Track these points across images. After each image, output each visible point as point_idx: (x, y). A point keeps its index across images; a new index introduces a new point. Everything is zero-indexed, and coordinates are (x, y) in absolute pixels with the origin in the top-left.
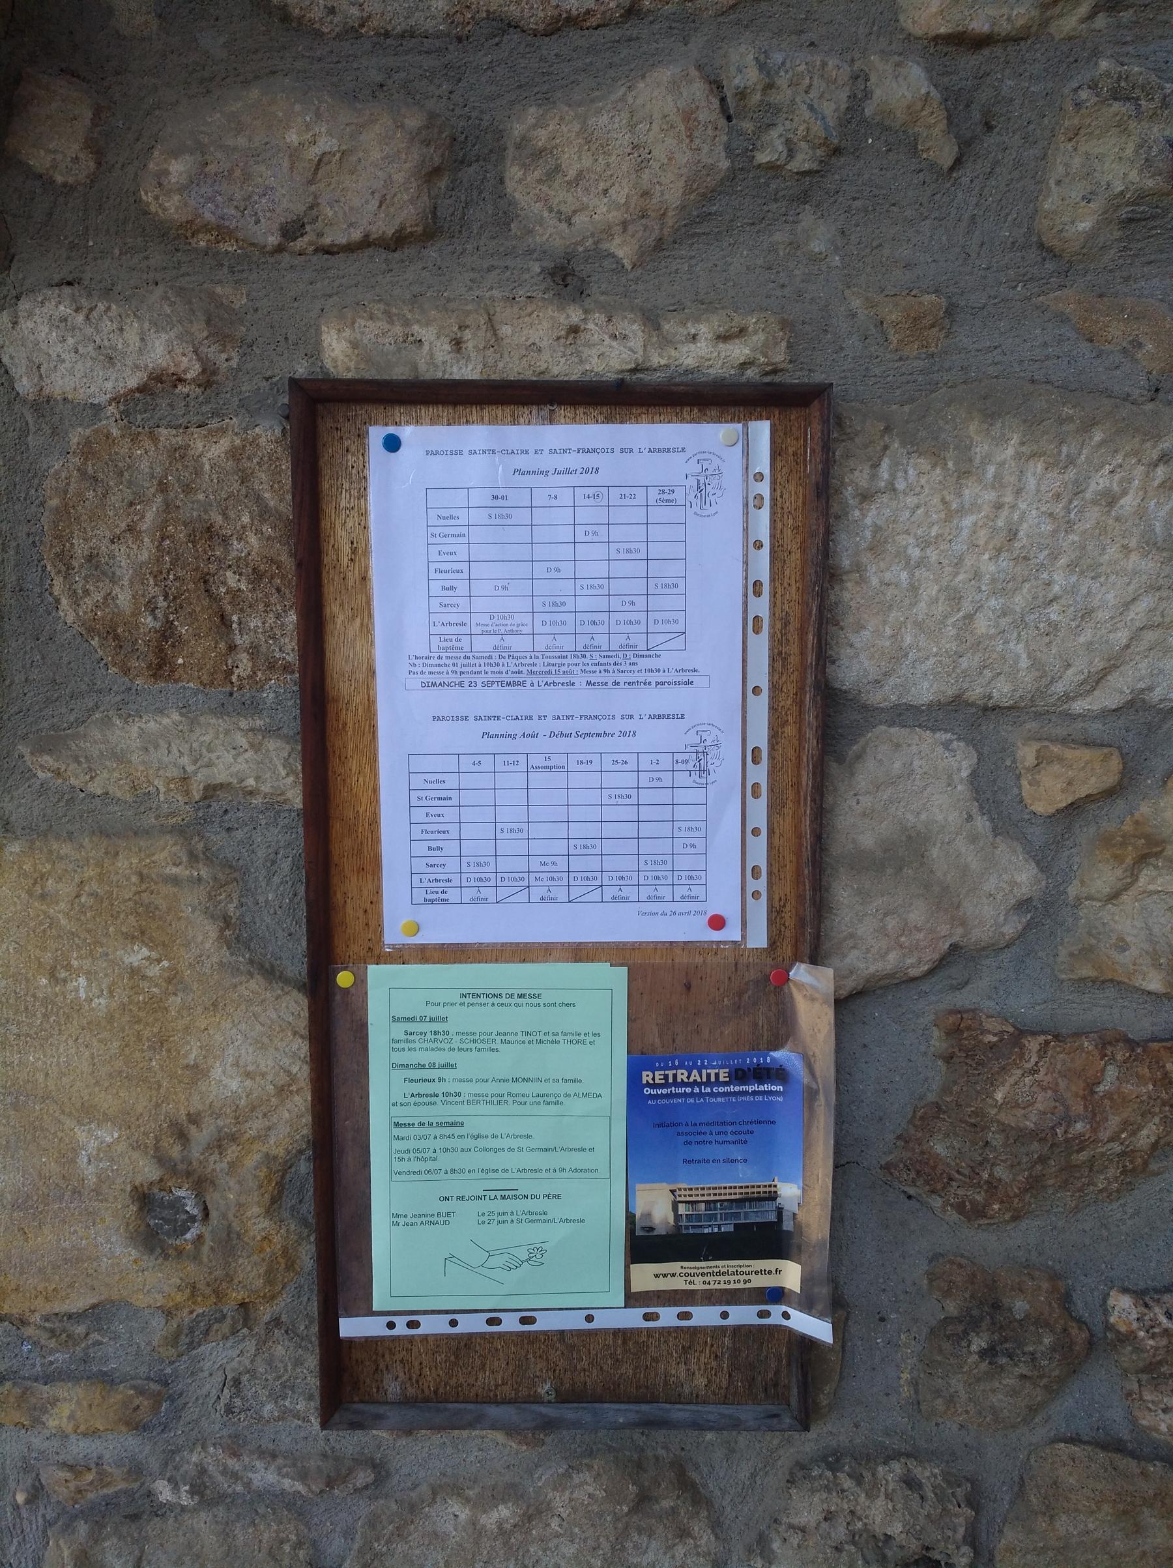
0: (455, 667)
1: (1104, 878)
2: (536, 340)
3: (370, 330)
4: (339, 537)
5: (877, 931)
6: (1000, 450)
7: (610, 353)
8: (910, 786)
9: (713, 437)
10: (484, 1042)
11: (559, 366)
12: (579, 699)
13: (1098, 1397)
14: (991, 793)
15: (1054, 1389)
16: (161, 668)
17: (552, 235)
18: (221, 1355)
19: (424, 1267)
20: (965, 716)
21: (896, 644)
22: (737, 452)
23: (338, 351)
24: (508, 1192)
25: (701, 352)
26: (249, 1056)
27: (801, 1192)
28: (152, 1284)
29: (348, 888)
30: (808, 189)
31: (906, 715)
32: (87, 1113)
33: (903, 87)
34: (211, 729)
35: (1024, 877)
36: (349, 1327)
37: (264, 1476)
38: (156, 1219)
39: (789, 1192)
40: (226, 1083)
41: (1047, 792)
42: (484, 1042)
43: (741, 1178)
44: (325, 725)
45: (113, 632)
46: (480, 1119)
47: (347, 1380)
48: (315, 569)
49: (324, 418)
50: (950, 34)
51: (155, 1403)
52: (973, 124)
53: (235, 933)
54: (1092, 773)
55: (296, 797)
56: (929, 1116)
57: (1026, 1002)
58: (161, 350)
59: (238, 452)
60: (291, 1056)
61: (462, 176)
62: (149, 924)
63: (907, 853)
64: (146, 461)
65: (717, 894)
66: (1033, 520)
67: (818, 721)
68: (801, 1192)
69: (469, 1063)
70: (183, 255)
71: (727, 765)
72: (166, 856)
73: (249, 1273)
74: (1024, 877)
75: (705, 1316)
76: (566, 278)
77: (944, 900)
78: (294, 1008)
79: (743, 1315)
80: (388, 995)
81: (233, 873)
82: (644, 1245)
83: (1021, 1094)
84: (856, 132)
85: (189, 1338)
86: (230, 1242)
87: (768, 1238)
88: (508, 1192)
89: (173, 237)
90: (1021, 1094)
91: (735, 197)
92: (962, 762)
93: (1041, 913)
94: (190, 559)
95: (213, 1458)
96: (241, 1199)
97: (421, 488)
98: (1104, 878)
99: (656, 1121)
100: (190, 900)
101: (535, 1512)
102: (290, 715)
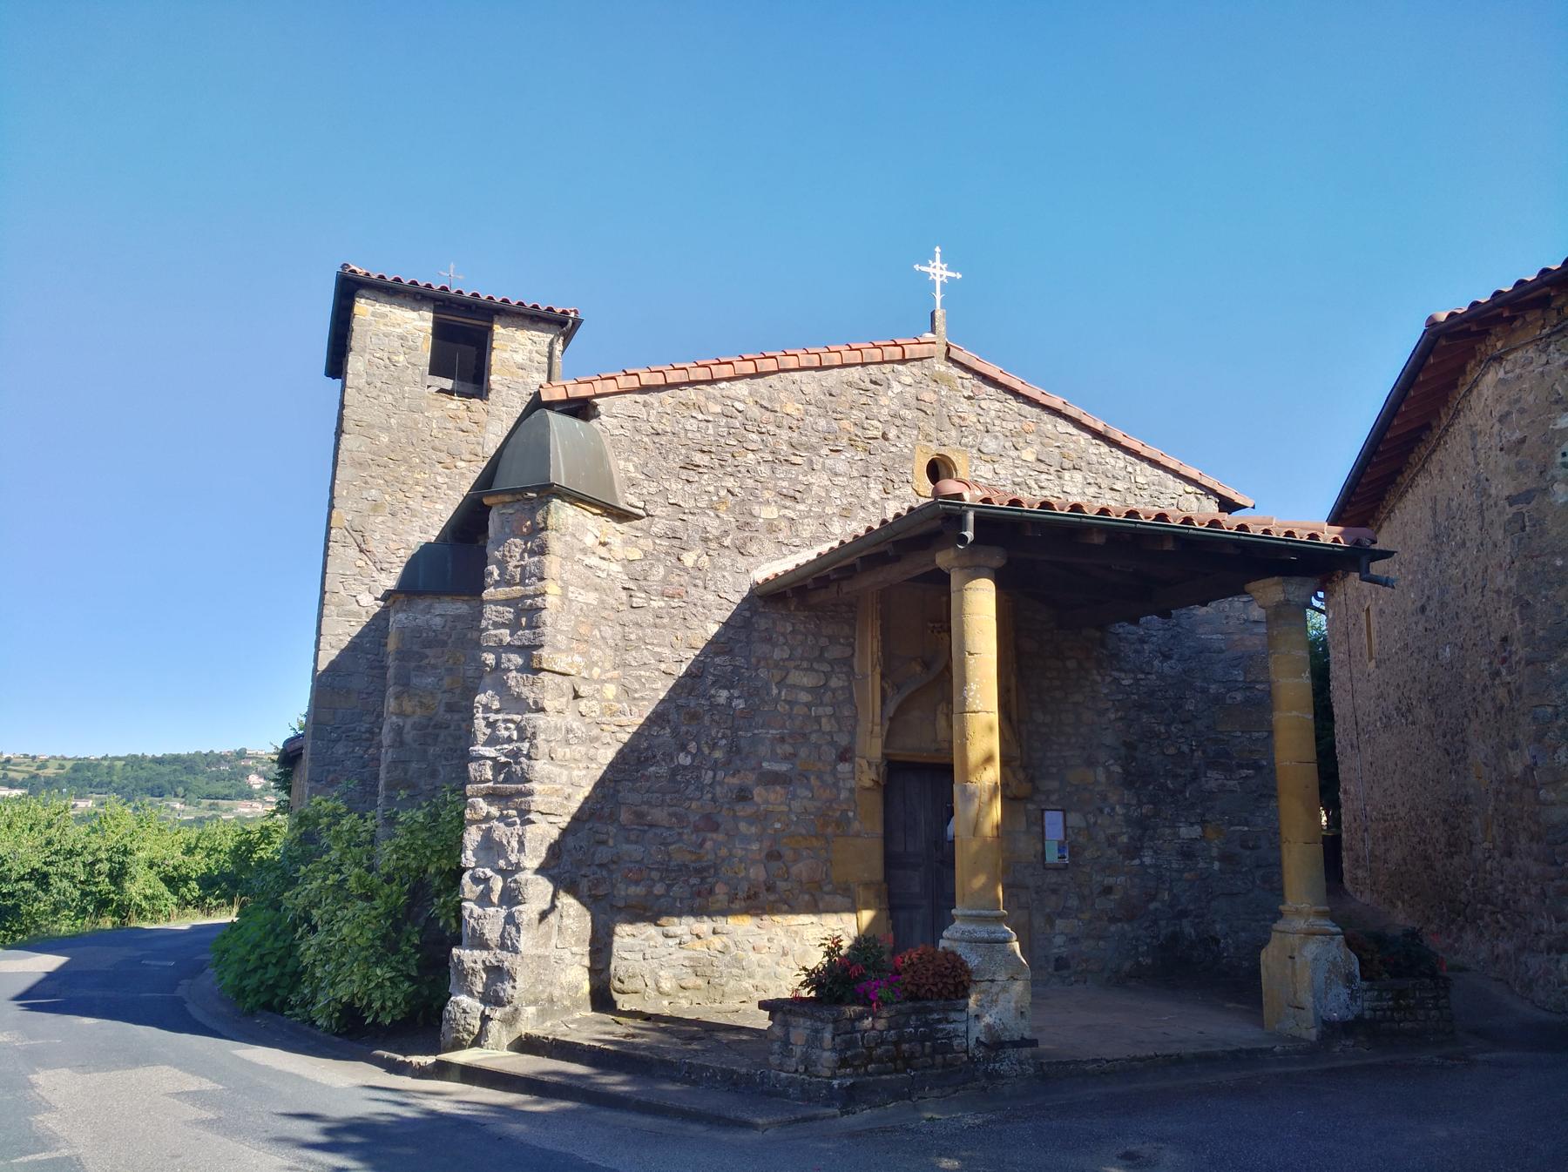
8: (1070, 831)
26: (1039, 847)
67: (1066, 827)
88: (1052, 856)
97: (1047, 814)
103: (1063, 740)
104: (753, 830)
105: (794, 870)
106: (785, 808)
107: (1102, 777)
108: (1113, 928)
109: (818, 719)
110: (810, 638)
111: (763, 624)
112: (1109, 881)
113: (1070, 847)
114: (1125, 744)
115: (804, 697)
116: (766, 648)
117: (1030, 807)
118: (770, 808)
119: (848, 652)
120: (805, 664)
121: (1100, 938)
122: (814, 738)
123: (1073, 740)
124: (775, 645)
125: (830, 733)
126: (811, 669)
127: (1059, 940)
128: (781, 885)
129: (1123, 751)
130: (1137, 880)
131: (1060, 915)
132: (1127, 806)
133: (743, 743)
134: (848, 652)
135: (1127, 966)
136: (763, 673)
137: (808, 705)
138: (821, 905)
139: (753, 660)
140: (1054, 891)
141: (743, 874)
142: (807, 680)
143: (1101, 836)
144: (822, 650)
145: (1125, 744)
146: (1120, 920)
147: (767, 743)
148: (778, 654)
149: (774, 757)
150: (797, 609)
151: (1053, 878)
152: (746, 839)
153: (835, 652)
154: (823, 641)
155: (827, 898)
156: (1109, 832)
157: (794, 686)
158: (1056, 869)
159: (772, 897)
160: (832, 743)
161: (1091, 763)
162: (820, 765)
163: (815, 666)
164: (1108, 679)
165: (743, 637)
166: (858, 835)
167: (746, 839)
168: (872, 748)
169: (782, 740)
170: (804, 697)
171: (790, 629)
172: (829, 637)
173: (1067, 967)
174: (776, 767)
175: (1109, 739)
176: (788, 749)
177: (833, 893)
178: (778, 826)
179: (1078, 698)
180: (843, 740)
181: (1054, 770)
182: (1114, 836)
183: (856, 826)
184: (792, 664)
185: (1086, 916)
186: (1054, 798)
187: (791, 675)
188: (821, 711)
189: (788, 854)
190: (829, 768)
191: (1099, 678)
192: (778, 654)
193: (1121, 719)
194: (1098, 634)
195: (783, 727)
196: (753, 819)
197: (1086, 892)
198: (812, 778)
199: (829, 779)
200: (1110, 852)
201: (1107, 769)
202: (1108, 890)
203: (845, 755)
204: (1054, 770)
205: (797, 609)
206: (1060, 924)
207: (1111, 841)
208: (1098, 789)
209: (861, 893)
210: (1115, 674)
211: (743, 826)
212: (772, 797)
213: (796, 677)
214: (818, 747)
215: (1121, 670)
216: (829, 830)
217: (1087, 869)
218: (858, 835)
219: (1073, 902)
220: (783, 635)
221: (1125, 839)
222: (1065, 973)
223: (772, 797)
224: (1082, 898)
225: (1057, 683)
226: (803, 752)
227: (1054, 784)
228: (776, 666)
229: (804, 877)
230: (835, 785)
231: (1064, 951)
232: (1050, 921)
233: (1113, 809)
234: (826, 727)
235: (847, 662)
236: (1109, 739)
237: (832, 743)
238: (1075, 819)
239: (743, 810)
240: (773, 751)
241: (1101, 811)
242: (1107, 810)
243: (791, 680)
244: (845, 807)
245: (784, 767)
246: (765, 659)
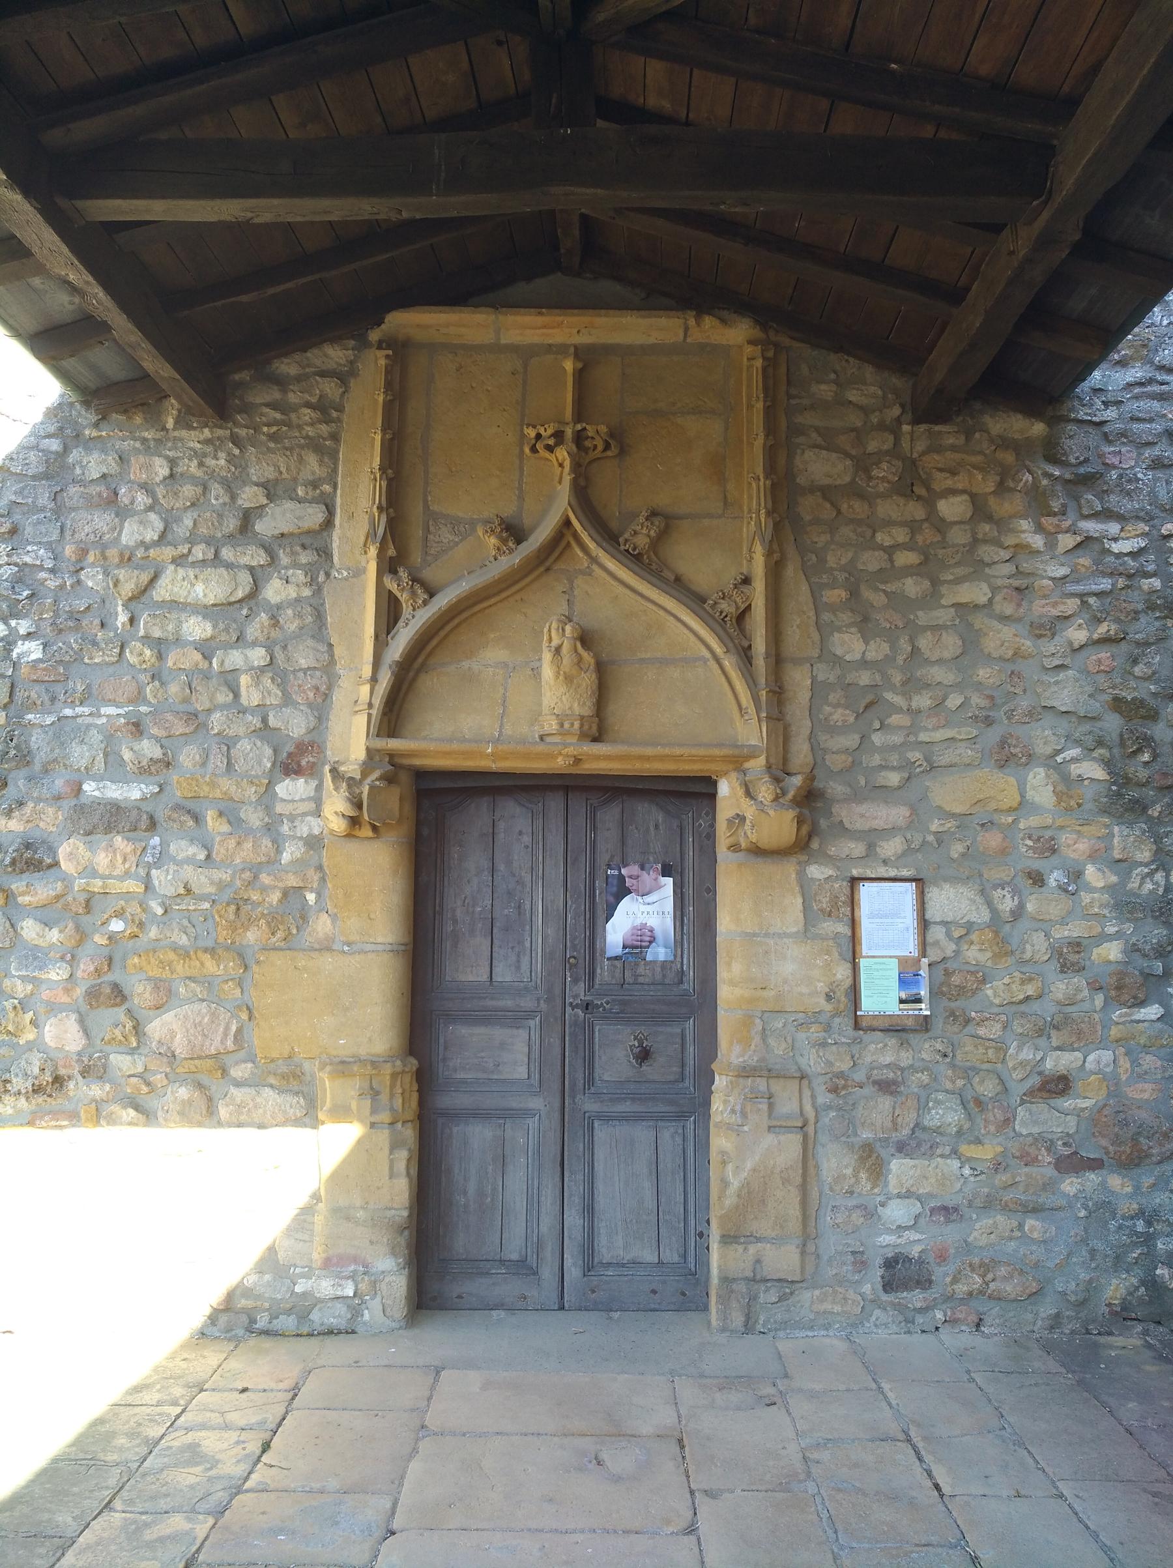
0: (872, 916)
1: (966, 947)
2: (882, 871)
3: (860, 870)
4: (856, 897)
5: (934, 954)
6: (947, 886)
7: (892, 873)
8: (937, 933)
9: (928, 896)
10: (878, 970)
11: (886, 875)
12: (890, 920)
13: (970, 1029)
14: (948, 934)
15: (964, 1026)
16: (830, 915)
17: (883, 856)
18: (837, 1020)
19: (870, 1004)
20: (944, 923)
21: (934, 912)
22: (911, 887)
23: (855, 873)
24: (881, 995)
25: (905, 873)
26: (842, 972)
27: (924, 993)
28: (829, 1007)
29: (857, 948)
30: (918, 850)
31: (935, 923)
32: (819, 981)
33: (931, 838)
34: (837, 925)
35: (954, 947)
36: (859, 1013)
37: (844, 1040)
38: (829, 998)
39: (922, 993)
40: (839, 976)
41: (956, 934)
42: (878, 970)
43: (914, 991)
44: (854, 924)
45: (822, 910)
46: (877, 981)
47: (857, 1026)
48: (853, 902)
49: (854, 881)
50: (839, 349)
51: (828, 1028)
52: (940, 842)
53: (840, 954)
54: (963, 932)
55: (849, 934)
56: (942, 984)
57: (955, 966)
58: (831, 872)
59: (841, 887)
60: (849, 972)
61: (871, 848)
62: (828, 953)
63: (937, 943)
64: (827, 886)
65: (910, 948)
66: (952, 896)
67: (924, 924)
68: (924, 993)
69: (876, 973)
70: (831, 860)
71: (911, 930)
72: (831, 943)
73: (842, 1006)
74: (954, 947)
75: (911, 1012)
76: (885, 862)
77: (943, 950)
78: (849, 965)
79: (916, 1012)
80: (863, 963)
81: (839, 945)
82: (902, 1001)
83: (956, 979)
84: (924, 843)
85: (833, 1016)
86: (839, 1001)
87: (918, 1000)
88: (881, 995)
89: (830, 857)
90: (956, 979)
91: (909, 851)
92: (944, 930)
93: (957, 953)
94: (834, 900)
95: (836, 1036)
96: (841, 995)
97: (867, 891)
98: (966, 947)
99: (903, 982)
100: (834, 949)
101: (886, 1045)
102: (850, 923)
103: (923, 701)
104: (54, 935)
105: (156, 1028)
106: (262, 921)
107: (1039, 785)
108: (1070, 1185)
109: (229, 679)
110: (216, 489)
111: (94, 464)
112: (1059, 1062)
113: (944, 987)
114: (1118, 704)
115: (196, 628)
116: (101, 521)
117: (816, 871)
118: (97, 885)
119: (314, 516)
120: (199, 552)
121: (1036, 1210)
122: (217, 721)
123: (954, 701)
124: (123, 513)
125: (262, 710)
126: (216, 560)
127: (897, 1212)
128: (121, 1062)
129: (1113, 723)
130: (1149, 1061)
131: (902, 1148)
132: (1122, 865)
133: (37, 740)
134: (314, 516)
135: (1116, 1288)
136: (93, 579)
137: (206, 649)
138: (223, 1112)
139: (69, 550)
140: (887, 1087)
141: (30, 1035)
142: (208, 588)
143: (1037, 946)
144: (247, 519)
145: (1118, 704)
146: (1095, 1165)
147: (95, 737)
148: (131, 533)
149: (114, 768)
150: (181, 423)
151: (883, 1054)
152: (37, 956)
153: (279, 519)
154: (249, 496)
155: (238, 1094)
156: (1062, 933)
157: (174, 605)
158: (894, 1028)
159: (97, 1091)
160: (265, 731)
161: (1008, 757)
162: (227, 785)
163: (227, 553)
164: (1067, 541)
165: (44, 499)
166: (326, 947)
167: (37, 956)
168: (351, 738)
169: (137, 728)
170: (196, 628)
171: (162, 471)
172: (264, 485)
173: (924, 1283)
174: (114, 792)
175: (1066, 693)
176: (149, 749)
177: (255, 1083)
178: (117, 926)
179: (977, 593)
180: (296, 725)
181: (894, 778)
182: (1077, 945)
183: (322, 925)
184: (168, 552)
185: (986, 1152)
186: (891, 847)
187: (164, 581)
188: (235, 658)
189: (141, 993)
190: (251, 792)
191: (1038, 541)
192: (131, 533)
193: (1106, 640)
194: (1038, 428)
195: (139, 697)
196: (47, 915)
197: (987, 1088)
198: (210, 816)
199: (254, 818)
200: (1061, 988)
201: (1061, 771)
202: (1057, 1086)
203: (295, 761)
204: (894, 778)
205: (181, 423)
206: (900, 1169)
207: (1070, 956)
208: (1034, 821)
209: (329, 1087)
210: (1091, 527)
211: (29, 929)
212: (102, 860)
213: (174, 584)
214: (228, 743)
215: (1107, 515)
216: (252, 936)
217: (992, 1030)
218: (326, 947)
219: (946, 1115)
220: (146, 487)
221: (1113, 951)
222: (916, 1298)
223: (102, 860)
224: (975, 1105)
225: (906, 558)
226: (188, 757)
227: (897, 814)
228: (127, 559)
229: (180, 1046)
230: (270, 828)
231: (915, 1243)
232: (871, 1160)
233: (1076, 875)
234: (251, 696)
235: (317, 541)
236: (1066, 693)
237: (265, 731)
238: (952, 902)
239: (34, 891)
240: (110, 754)
241: (1038, 879)
242: (1054, 878)
243: (163, 591)
244: (292, 881)
245: (134, 792)
246: (103, 547)
